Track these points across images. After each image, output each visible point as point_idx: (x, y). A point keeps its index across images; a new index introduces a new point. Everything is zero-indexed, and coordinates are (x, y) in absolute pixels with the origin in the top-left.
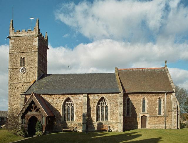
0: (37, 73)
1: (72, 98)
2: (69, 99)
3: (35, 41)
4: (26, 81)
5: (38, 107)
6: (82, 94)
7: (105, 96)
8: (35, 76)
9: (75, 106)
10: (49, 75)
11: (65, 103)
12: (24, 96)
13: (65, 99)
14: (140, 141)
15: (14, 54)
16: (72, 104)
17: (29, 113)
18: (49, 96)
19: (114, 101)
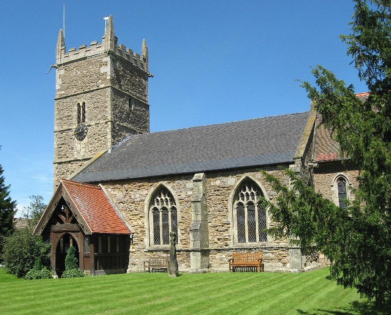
7: (253, 176)
9: (178, 206)
13: (152, 189)
17: (58, 226)
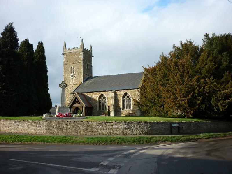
1: (104, 94)
2: (102, 95)
3: (81, 55)
4: (75, 84)
5: (80, 101)
8: (81, 79)
9: (107, 100)
10: (95, 77)
11: (124, 97)
12: (72, 94)
13: (99, 95)
16: (105, 98)
17: (75, 105)
18: (88, 93)
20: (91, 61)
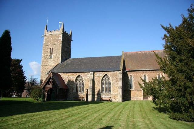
0: (60, 58)
6: (90, 72)
9: (84, 81)
13: (77, 76)
14: (32, 112)
15: (46, 46)
16: (82, 80)
18: (65, 74)
19: (116, 77)
20: (70, 44)
